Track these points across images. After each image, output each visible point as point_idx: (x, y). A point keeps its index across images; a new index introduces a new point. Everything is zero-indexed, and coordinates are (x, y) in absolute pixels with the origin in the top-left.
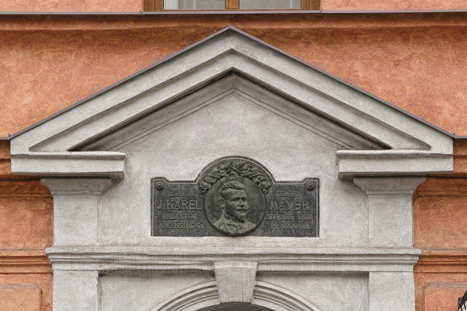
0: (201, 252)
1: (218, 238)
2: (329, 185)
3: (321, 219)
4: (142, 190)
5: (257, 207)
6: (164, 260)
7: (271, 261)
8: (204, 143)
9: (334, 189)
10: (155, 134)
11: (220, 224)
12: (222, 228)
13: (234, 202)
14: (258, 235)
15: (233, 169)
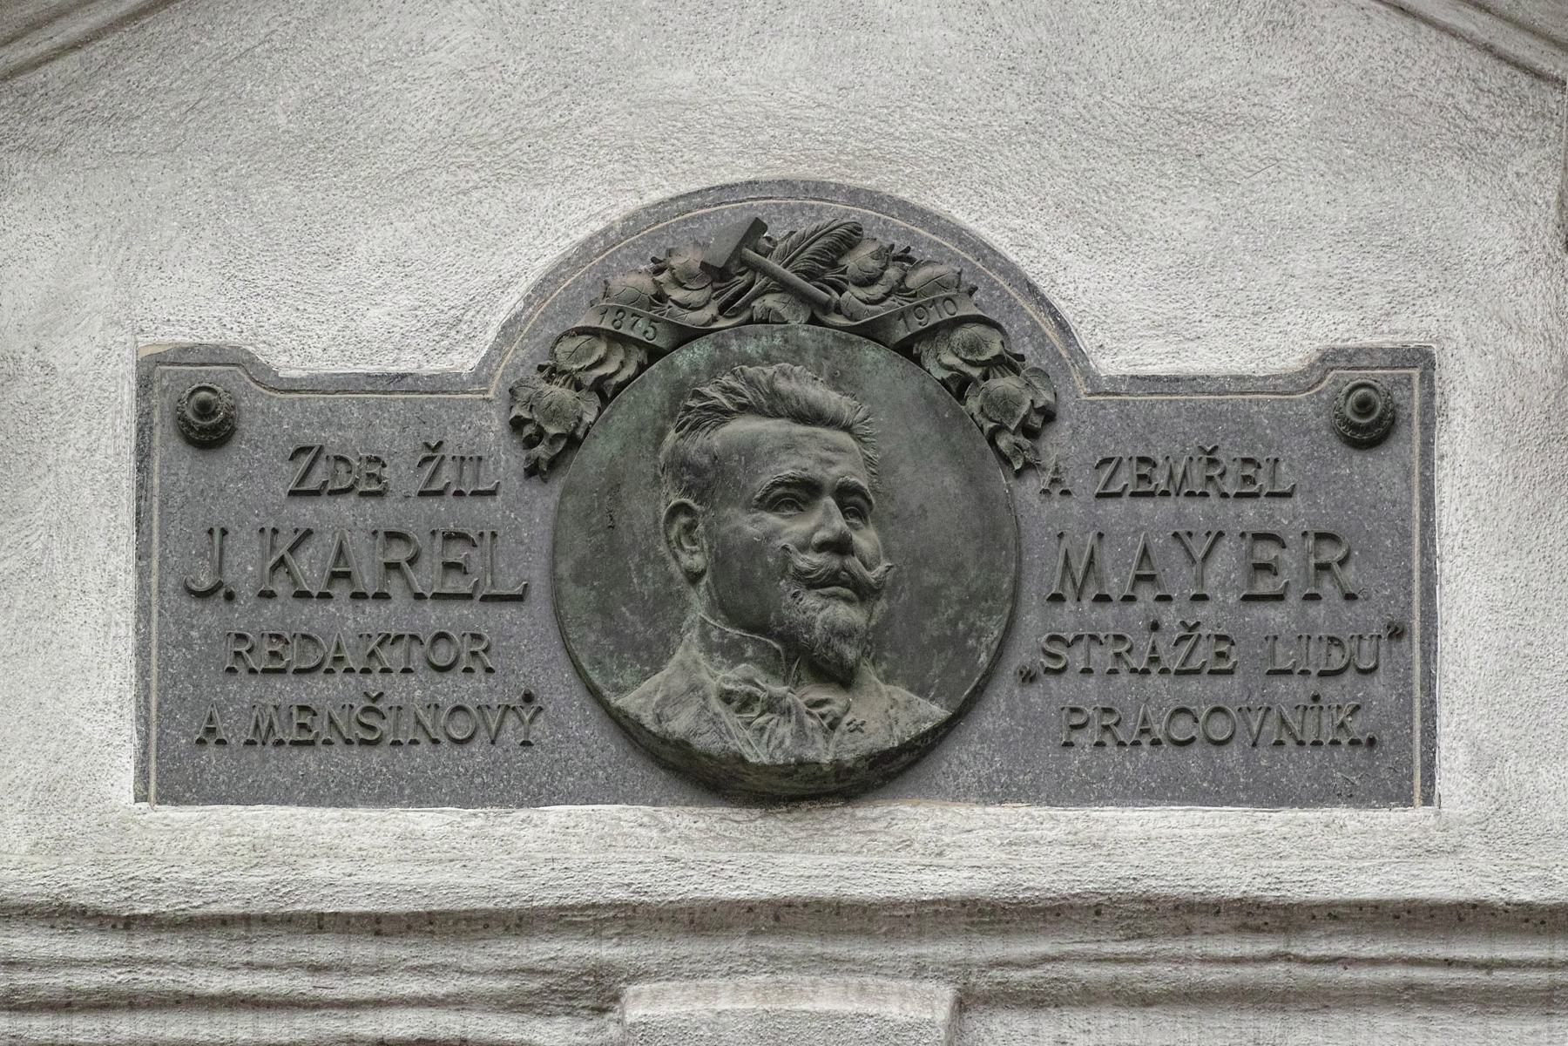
0: (515, 887)
1: (652, 816)
2: (1510, 403)
3: (1446, 667)
4: (71, 452)
5: (957, 570)
6: (231, 968)
7: (1062, 970)
8: (544, 93)
9: (1548, 440)
10: (171, 28)
11: (665, 698)
12: (680, 724)
13: (772, 519)
14: (960, 795)
15: (766, 272)
